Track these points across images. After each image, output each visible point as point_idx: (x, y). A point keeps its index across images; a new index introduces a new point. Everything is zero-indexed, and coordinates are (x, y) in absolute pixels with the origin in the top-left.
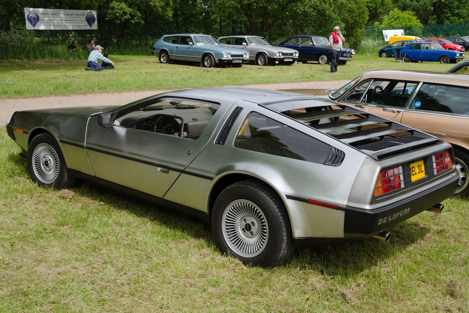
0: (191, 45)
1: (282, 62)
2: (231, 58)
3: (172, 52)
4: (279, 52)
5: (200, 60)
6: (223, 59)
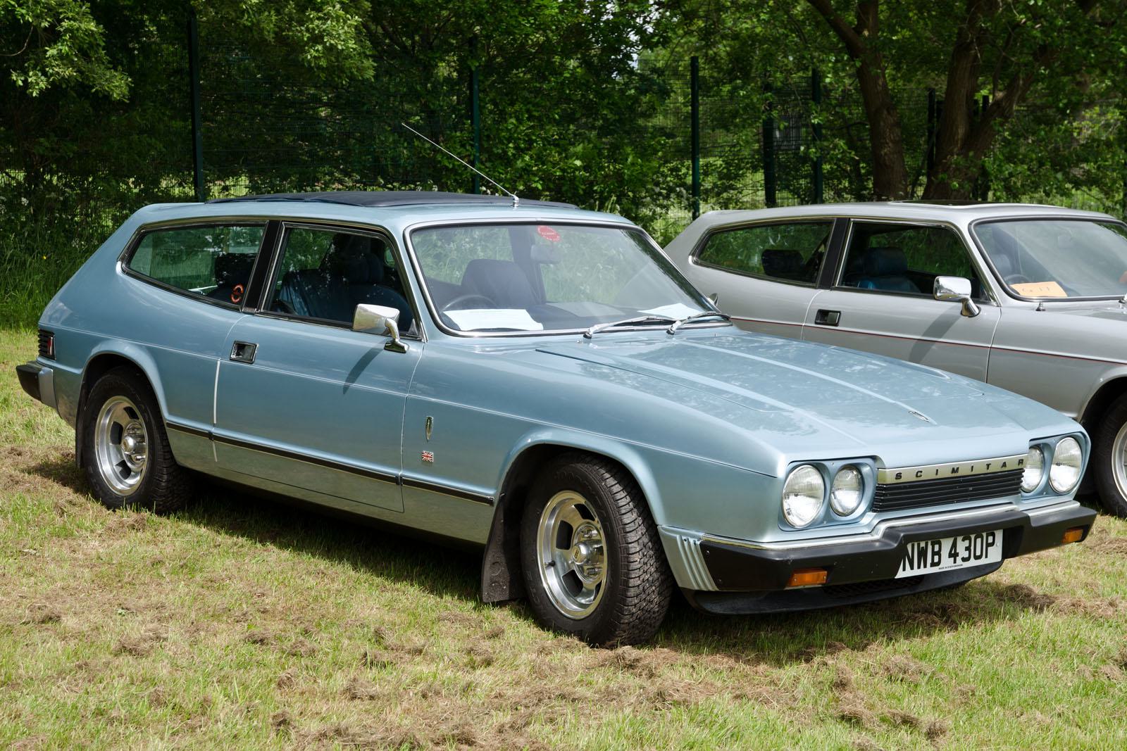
0: (388, 332)
2: (868, 528)
3: (190, 378)
5: (476, 528)
6: (772, 542)
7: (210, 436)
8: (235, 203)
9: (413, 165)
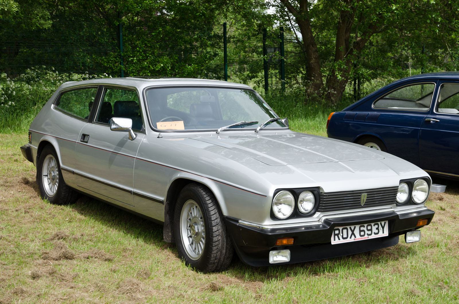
1: (313, 251)
4: (296, 193)
5: (159, 214)
7: (73, 173)
8: (76, 81)
9: (93, 66)
